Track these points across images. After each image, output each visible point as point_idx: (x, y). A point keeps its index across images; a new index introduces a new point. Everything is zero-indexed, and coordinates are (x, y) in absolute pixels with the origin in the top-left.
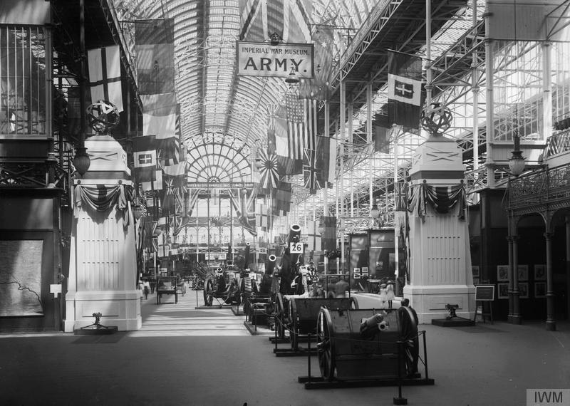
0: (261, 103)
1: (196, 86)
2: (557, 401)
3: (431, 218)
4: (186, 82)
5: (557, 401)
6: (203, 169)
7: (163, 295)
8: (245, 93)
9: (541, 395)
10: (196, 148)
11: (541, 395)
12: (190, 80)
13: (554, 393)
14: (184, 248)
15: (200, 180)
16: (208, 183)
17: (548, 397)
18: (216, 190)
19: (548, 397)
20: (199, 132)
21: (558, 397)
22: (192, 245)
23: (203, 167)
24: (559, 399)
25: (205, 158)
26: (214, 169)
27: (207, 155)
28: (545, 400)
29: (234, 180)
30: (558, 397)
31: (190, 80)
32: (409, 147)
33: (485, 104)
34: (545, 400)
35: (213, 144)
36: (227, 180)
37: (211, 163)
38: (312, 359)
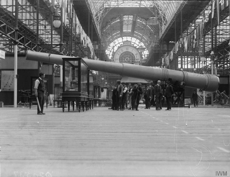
2: (225, 175)
9: (218, 173)
11: (218, 173)
13: (224, 172)
21: (225, 173)
28: (220, 174)
30: (225, 173)
32: (227, 24)
34: (220, 174)
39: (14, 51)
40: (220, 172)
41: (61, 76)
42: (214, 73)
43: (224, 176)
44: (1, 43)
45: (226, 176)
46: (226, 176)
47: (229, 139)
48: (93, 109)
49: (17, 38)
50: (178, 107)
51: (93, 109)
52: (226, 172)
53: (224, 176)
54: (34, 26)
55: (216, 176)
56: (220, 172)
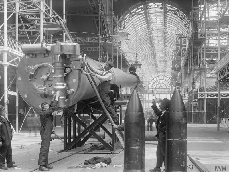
0: (179, 28)
1: (149, 39)
2: (224, 170)
4: (145, 43)
5: (224, 170)
6: (162, 83)
7: (41, 166)
8: (170, 23)
10: (156, 77)
13: (223, 167)
15: (157, 88)
16: (156, 89)
18: (224, 72)
20: (139, 66)
21: (224, 168)
23: (160, 82)
25: (158, 81)
26: (159, 85)
28: (219, 169)
30: (224, 168)
31: (147, 43)
34: (219, 169)
36: (166, 87)
37: (158, 83)
38: (217, 41)
39: (145, 97)
40: (219, 167)
41: (5, 32)
42: (43, 24)
44: (83, 56)
45: (226, 171)
46: (226, 171)
47: (205, 124)
48: (36, 57)
49: (117, 141)
50: (80, 47)
51: (36, 57)
52: (225, 167)
53: (220, 171)
54: (201, 7)
55: (215, 171)
56: (219, 167)
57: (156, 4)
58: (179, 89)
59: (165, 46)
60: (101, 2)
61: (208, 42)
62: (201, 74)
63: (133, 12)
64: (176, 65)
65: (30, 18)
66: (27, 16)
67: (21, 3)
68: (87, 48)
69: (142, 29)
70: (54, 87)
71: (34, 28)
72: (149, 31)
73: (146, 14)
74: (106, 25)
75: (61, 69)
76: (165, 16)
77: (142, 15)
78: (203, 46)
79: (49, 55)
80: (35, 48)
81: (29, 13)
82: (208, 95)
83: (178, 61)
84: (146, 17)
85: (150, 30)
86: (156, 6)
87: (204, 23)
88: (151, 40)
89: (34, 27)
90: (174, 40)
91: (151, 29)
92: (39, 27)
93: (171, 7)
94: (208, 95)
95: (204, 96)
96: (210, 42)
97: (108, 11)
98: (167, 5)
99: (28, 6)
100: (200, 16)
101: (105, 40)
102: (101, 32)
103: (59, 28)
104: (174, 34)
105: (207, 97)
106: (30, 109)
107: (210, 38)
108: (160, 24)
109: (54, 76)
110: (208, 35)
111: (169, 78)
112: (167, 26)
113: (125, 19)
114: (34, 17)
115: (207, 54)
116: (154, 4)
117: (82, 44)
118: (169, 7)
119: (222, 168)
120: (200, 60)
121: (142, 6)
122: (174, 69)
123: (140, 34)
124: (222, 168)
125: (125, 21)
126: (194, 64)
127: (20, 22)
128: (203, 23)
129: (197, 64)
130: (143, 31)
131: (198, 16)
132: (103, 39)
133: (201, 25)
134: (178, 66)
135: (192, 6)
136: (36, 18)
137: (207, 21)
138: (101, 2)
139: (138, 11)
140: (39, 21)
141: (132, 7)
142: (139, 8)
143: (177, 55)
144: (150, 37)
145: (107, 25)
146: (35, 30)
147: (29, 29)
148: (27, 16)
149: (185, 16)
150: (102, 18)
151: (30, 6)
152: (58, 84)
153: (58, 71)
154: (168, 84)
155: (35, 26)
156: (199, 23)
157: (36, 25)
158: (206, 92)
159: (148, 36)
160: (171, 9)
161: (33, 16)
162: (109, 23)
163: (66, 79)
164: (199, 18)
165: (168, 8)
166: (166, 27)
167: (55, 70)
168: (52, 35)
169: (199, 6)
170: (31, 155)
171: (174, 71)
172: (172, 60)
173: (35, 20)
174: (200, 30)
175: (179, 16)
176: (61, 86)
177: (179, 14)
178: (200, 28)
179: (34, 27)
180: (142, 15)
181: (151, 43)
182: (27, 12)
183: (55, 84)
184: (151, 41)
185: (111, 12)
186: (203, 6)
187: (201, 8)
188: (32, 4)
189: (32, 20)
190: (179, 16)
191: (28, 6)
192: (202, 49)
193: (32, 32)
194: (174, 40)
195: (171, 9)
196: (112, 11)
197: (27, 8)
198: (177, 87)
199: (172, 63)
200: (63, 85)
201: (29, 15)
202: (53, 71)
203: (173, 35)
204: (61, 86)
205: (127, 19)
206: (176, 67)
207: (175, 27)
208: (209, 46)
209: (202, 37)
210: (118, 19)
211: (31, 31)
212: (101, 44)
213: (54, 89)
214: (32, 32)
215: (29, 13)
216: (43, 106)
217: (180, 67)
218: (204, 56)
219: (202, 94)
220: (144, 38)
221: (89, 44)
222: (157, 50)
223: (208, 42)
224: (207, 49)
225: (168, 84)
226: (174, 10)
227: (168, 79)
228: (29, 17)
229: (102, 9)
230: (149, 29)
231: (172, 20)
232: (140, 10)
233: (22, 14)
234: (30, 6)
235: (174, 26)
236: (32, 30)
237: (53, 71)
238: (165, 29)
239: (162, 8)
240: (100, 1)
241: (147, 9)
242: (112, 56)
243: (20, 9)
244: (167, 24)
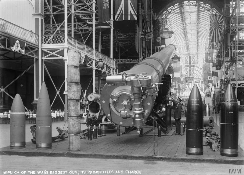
1: (180, 17)
3: (207, 97)
4: (175, 19)
5: (239, 173)
9: (232, 170)
11: (232, 170)
12: (178, 20)
13: (237, 170)
14: (184, 98)
17: (235, 171)
19: (235, 171)
21: (239, 171)
22: (186, 97)
24: (239, 171)
27: (199, 72)
29: (199, 77)
30: (239, 171)
31: (177, 18)
33: (204, 145)
34: (239, 170)
35: (199, 68)
36: (197, 77)
43: (238, 174)
52: (240, 170)
57: (190, 1)
58: (211, 79)
59: (198, 40)
60: (141, 1)
61: (239, 36)
62: (232, 65)
63: (169, 10)
64: (208, 57)
65: (83, 18)
66: (81, 16)
67: (76, 5)
68: (128, 43)
69: (177, 24)
70: (134, 111)
71: (85, 27)
72: (184, 27)
73: (182, 13)
74: (145, 21)
75: (139, 98)
76: (198, 14)
77: (177, 14)
78: (235, 39)
79: (128, 84)
80: (198, 163)
81: (83, 14)
82: (239, 85)
83: (211, 54)
84: (182, 15)
85: (185, 25)
86: (190, 3)
87: (235, 19)
88: (185, 34)
89: (86, 26)
90: (207, 34)
91: (185, 24)
92: (92, 26)
93: (204, 4)
94: (239, 85)
95: (235, 85)
96: (241, 36)
97: (147, 9)
98: (201, 2)
99: (82, 8)
100: (231, 12)
101: (145, 36)
102: (141, 28)
103: (107, 26)
104: (206, 29)
105: (238, 86)
106: (59, 90)
107: (241, 32)
108: (194, 21)
109: (134, 104)
110: (239, 30)
111: (201, 69)
112: (200, 21)
113: (162, 16)
114: (86, 17)
115: (238, 46)
116: (189, 1)
117: (124, 39)
118: (202, 4)
119: (236, 170)
120: (231, 52)
121: (178, 4)
122: (207, 61)
123: (175, 29)
124: (236, 170)
125: (162, 17)
126: (226, 57)
127: (75, 22)
128: (234, 18)
129: (229, 56)
130: (178, 26)
131: (230, 12)
132: (143, 34)
133: (232, 20)
134: (210, 58)
135: (224, 3)
136: (88, 18)
137: (238, 17)
138: (141, 1)
139: (174, 9)
140: (91, 20)
141: (169, 5)
142: (175, 6)
143: (210, 48)
144: (184, 32)
145: (146, 21)
146: (86, 28)
147: (82, 27)
148: (81, 16)
149: (217, 12)
150: (142, 16)
151: (84, 8)
152: (137, 109)
153: (137, 100)
154: (200, 74)
155: (87, 25)
156: (231, 18)
157: (87, 24)
158: (237, 82)
159: (182, 30)
160: (204, 6)
161: (85, 16)
162: (148, 20)
163: (142, 106)
164: (231, 14)
165: (202, 5)
166: (199, 22)
167: (134, 98)
168: (101, 33)
169: (231, 2)
170: (169, 168)
171: (206, 62)
172: (204, 52)
173: (87, 19)
174: (232, 25)
175: (211, 12)
176: (138, 111)
177: (212, 10)
178: (231, 24)
179: (86, 26)
180: (177, 14)
181: (182, 19)
182: (81, 13)
183: (135, 109)
184: (185, 36)
185: (150, 10)
186: (234, 3)
187: (233, 4)
188: (86, 6)
189: (85, 20)
190: (211, 12)
191: (82, 8)
192: (234, 42)
193: (83, 30)
194: (207, 34)
195: (204, 6)
196: (150, 9)
197: (81, 10)
198: (210, 77)
199: (204, 55)
200: (140, 110)
201: (82, 15)
202: (133, 99)
203: (205, 30)
204: (138, 111)
205: (163, 16)
206: (208, 59)
207: (207, 22)
208: (240, 40)
209: (234, 31)
210: (156, 16)
211: (82, 30)
212: (141, 39)
213: (134, 113)
214: (83, 30)
215: (83, 14)
216: (185, 160)
217: (212, 59)
218: (235, 49)
219: (233, 84)
220: (178, 32)
221: (130, 39)
222: (190, 43)
223: (239, 36)
224: (238, 42)
225: (200, 74)
226: (207, 6)
227: (199, 69)
228: (82, 17)
229: (142, 7)
230: (183, 24)
231: (205, 17)
232: (176, 7)
233: (77, 15)
234: (84, 8)
235: (207, 21)
236: (83, 29)
237: (133, 99)
238: (198, 24)
239: (196, 5)
240: (140, 0)
241: (182, 6)
242: (151, 49)
243: (75, 10)
244: (200, 20)
